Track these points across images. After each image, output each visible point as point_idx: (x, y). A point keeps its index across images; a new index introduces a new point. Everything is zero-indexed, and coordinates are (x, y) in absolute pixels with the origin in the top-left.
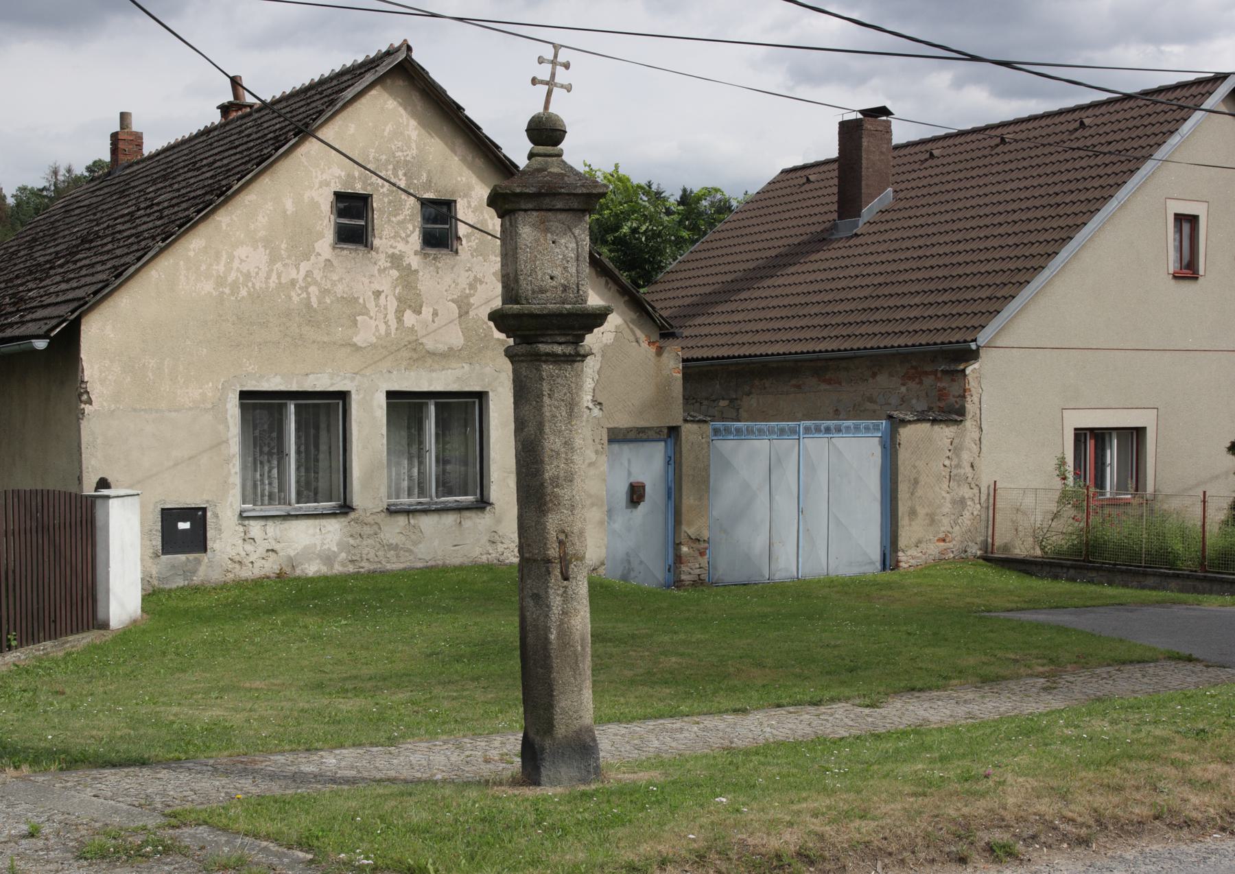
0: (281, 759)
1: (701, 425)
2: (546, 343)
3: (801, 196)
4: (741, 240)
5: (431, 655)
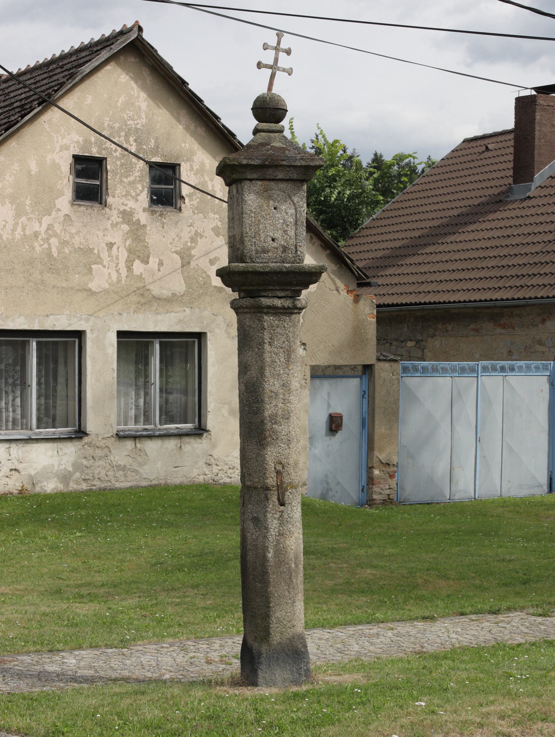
0: (27, 659)
1: (392, 364)
2: (268, 297)
3: (480, 163)
4: (427, 201)
5: (156, 564)
